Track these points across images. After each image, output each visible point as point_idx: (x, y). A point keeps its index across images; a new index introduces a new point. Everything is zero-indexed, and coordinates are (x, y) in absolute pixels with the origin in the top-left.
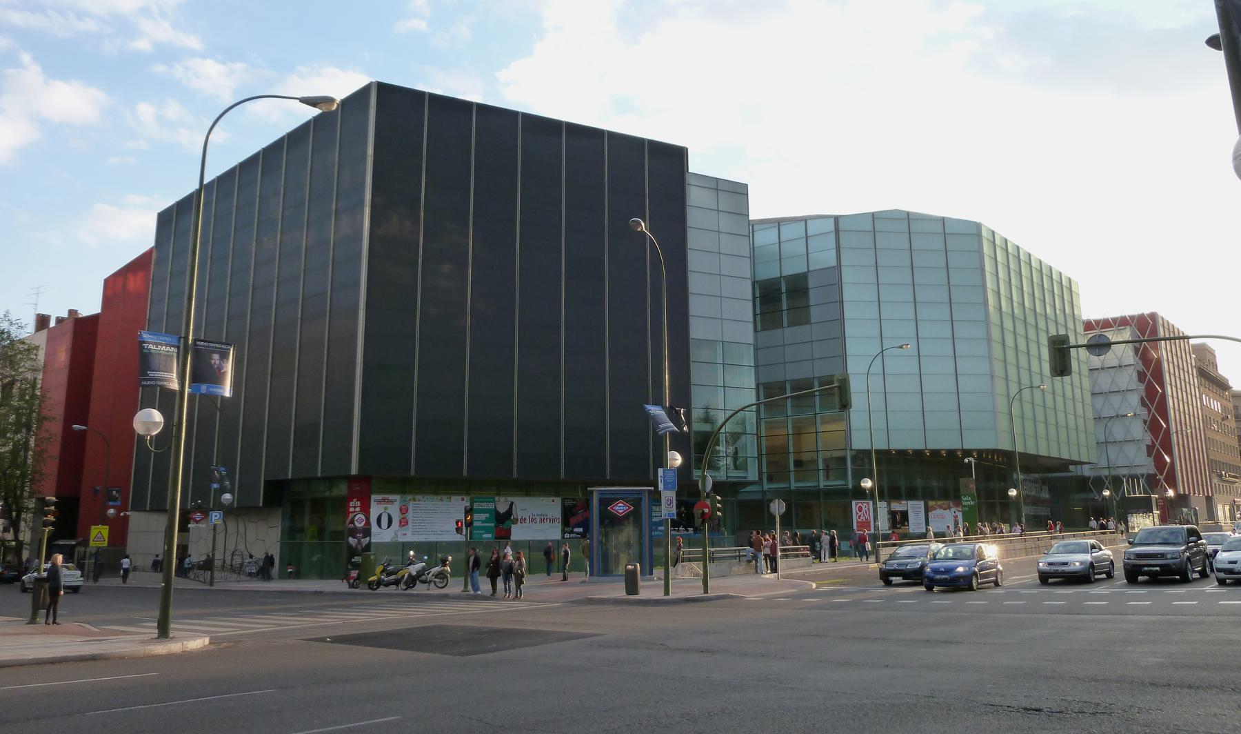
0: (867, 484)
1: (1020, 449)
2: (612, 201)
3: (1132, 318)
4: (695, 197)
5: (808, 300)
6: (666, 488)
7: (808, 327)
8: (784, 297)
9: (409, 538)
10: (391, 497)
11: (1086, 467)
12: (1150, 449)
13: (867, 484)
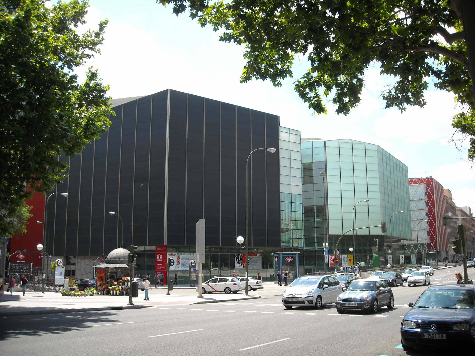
0: (351, 249)
3: (424, 179)
9: (180, 269)
10: (174, 253)
12: (429, 233)
13: (351, 249)
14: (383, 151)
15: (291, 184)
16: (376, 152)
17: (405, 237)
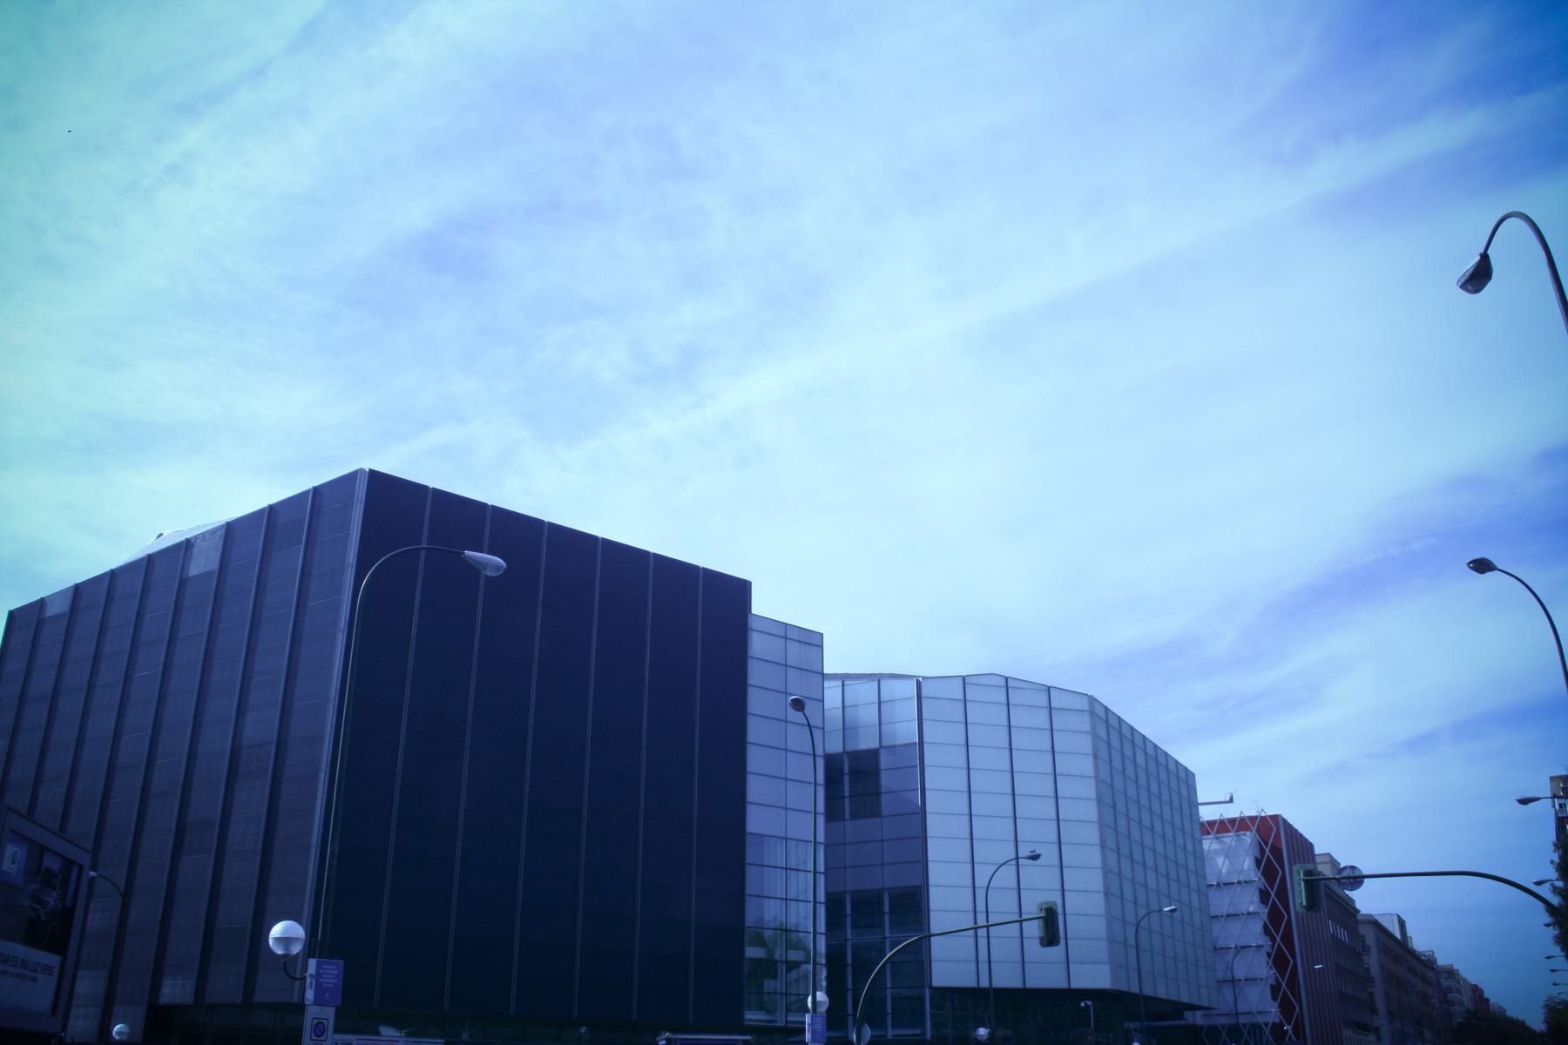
1: (1148, 991)
2: (664, 646)
4: (758, 645)
5: (877, 784)
6: (318, 1001)
7: (877, 820)
8: (846, 779)
11: (1199, 1013)
12: (1275, 990)
14: (1149, 746)
15: (782, 809)
16: (1086, 718)
17: (1195, 1002)
